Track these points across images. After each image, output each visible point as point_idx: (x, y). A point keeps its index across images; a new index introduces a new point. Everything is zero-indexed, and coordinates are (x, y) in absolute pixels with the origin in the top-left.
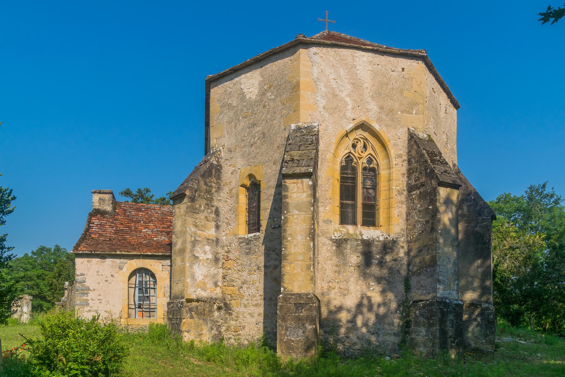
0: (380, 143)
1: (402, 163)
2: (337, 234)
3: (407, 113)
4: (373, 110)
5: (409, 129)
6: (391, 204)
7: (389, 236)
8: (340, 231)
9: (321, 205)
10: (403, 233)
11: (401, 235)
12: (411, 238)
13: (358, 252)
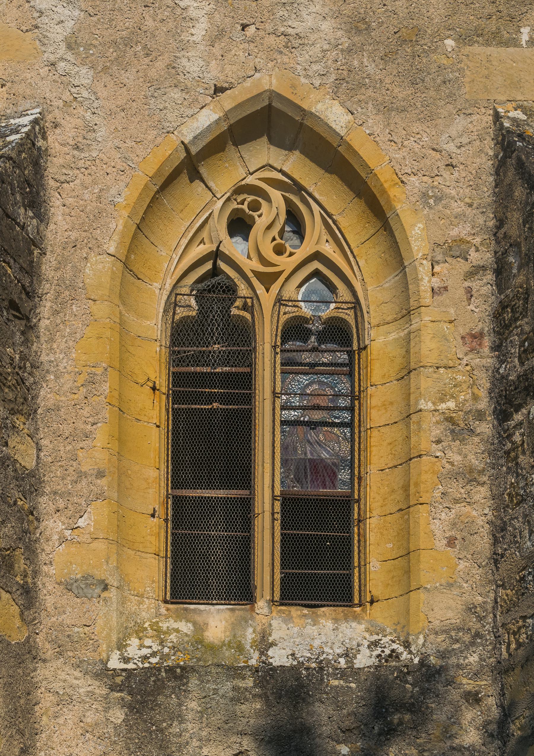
0: (359, 195)
1: (467, 284)
2: (141, 646)
3: (487, 44)
4: (312, 37)
5: (497, 116)
6: (417, 484)
7: (407, 645)
8: (159, 631)
9: (52, 508)
10: (473, 624)
11: (467, 638)
12: (513, 646)
13: (242, 734)
